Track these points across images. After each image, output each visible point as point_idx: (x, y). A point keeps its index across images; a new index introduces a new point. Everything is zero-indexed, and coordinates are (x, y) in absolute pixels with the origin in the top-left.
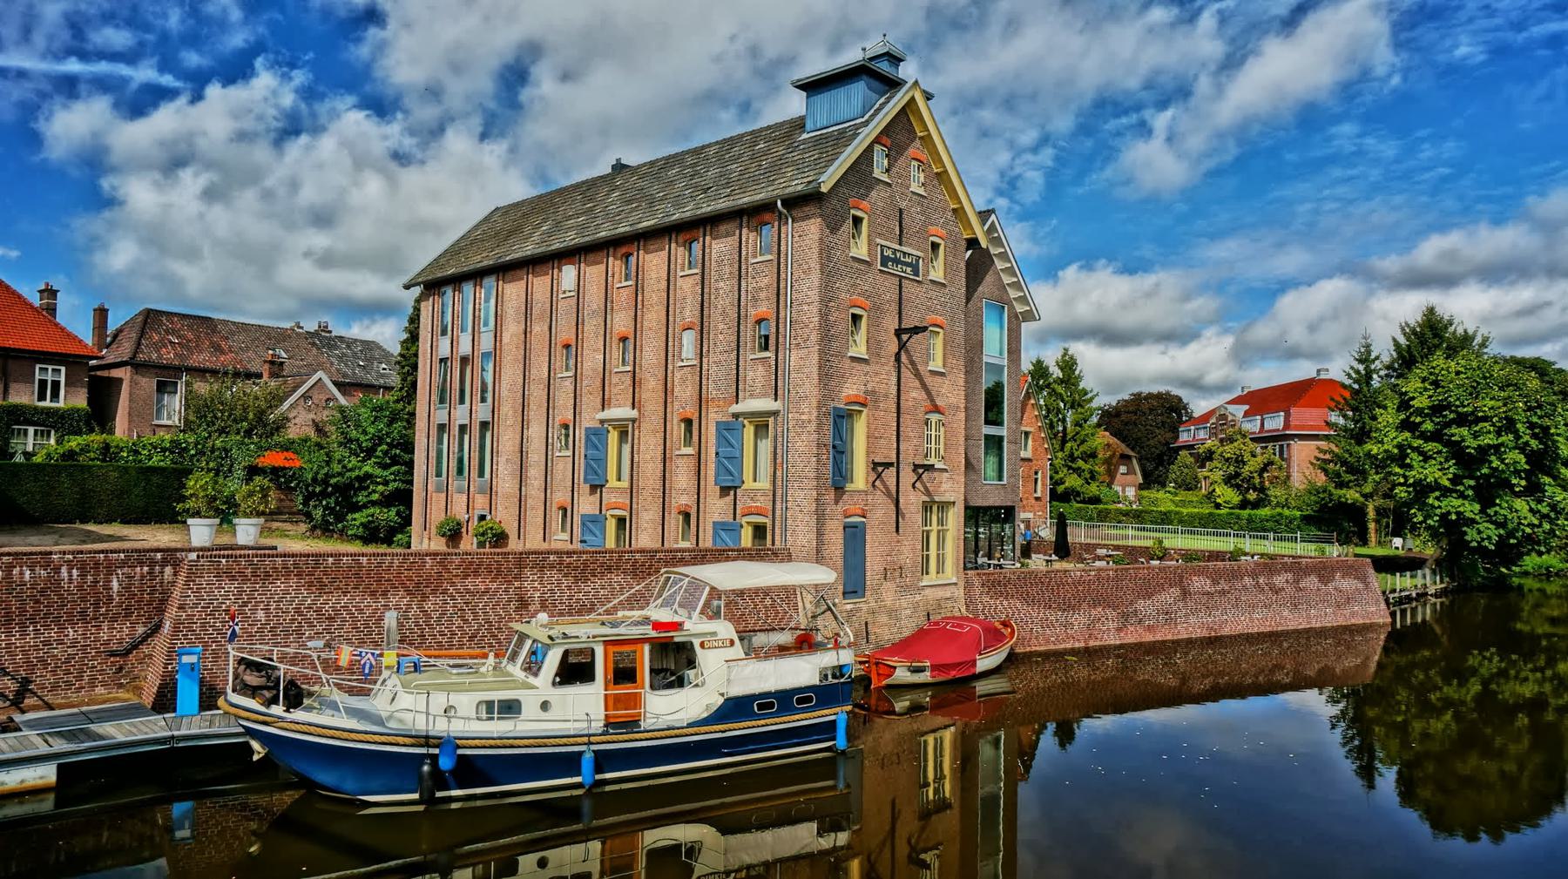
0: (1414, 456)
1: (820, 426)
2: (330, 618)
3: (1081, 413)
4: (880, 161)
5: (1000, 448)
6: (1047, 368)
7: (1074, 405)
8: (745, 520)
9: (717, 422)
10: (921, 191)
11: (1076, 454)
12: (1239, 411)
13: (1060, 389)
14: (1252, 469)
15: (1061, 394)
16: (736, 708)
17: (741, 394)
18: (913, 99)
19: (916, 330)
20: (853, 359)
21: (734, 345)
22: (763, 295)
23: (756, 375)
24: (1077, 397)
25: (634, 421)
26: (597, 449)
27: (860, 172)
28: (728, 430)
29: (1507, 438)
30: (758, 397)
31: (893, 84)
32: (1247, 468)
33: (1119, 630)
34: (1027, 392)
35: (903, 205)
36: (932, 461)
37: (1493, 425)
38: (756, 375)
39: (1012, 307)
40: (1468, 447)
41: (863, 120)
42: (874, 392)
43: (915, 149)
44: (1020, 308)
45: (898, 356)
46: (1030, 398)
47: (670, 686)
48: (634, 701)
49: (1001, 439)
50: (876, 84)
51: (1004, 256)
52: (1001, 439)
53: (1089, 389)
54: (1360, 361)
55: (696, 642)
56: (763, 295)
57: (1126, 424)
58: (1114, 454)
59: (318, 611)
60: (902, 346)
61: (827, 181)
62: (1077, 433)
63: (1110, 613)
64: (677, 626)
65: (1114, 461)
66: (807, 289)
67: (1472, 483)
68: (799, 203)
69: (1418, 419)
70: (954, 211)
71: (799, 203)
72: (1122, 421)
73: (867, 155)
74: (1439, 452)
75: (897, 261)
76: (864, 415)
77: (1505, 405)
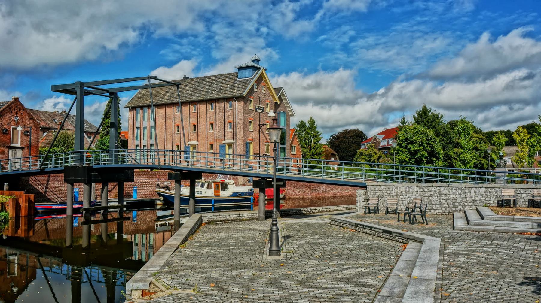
0: (400, 153)
1: (243, 146)
2: (152, 184)
3: (316, 139)
4: (255, 86)
5: (284, 151)
6: (305, 123)
7: (314, 137)
8: (226, 166)
9: (220, 145)
10: (264, 92)
11: (315, 153)
12: (381, 137)
13: (309, 131)
14: (374, 158)
15: (309, 133)
16: (235, 194)
17: (225, 139)
18: (263, 72)
19: (263, 125)
20: (250, 131)
21: (223, 128)
22: (230, 117)
23: (229, 135)
24: (315, 134)
25: (197, 144)
26: (223, 150)
27: (251, 91)
28: (222, 147)
29: (422, 148)
30: (229, 139)
31: (257, 69)
32: (373, 158)
33: (311, 194)
34: (295, 134)
35: (260, 96)
36: (267, 153)
37: (418, 144)
38: (229, 135)
39: (288, 113)
40: (412, 150)
41: (252, 78)
42: (254, 138)
43: (263, 83)
44: (290, 113)
45: (259, 130)
46: (295, 136)
47: (223, 191)
48: (219, 192)
49: (284, 148)
50: (256, 69)
51: (285, 99)
52: (284, 148)
53: (319, 131)
54: (402, 123)
55: (228, 183)
56: (230, 117)
57: (341, 142)
58: (329, 153)
59: (149, 182)
60: (260, 128)
61: (245, 94)
62: (315, 146)
63: (309, 190)
64: (224, 181)
65: (329, 156)
66: (240, 117)
67: (414, 160)
68: (239, 98)
69: (401, 143)
70: (272, 96)
71: (239, 98)
72: (339, 141)
73: (253, 87)
74: (406, 152)
75: (259, 109)
76: (252, 144)
77: (421, 139)
